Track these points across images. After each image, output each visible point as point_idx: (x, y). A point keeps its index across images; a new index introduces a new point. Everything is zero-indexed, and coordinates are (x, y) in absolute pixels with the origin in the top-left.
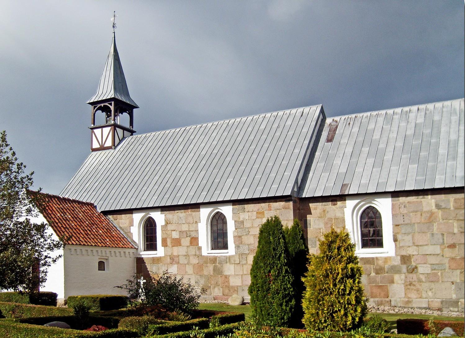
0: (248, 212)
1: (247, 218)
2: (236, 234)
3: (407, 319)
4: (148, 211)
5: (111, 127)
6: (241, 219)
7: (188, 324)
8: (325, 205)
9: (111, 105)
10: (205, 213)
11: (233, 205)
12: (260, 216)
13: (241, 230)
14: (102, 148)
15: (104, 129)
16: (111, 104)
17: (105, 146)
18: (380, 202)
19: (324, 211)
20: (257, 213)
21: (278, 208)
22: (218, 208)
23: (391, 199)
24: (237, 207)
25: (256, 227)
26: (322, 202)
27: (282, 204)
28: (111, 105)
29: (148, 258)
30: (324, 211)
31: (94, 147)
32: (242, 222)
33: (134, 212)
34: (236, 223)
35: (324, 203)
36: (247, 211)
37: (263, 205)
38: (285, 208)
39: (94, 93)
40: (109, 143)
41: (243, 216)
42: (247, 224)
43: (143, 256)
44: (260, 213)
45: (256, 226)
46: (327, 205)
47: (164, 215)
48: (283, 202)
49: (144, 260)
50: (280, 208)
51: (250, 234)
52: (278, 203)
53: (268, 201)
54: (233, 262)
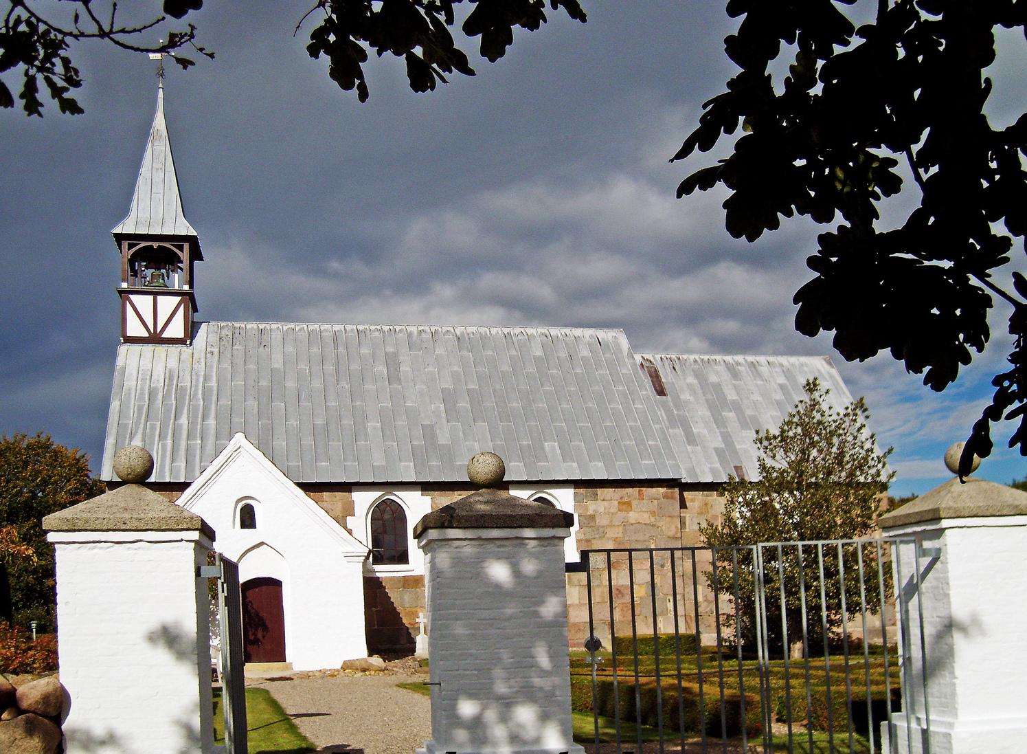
0: (604, 500)
1: (602, 510)
2: (582, 537)
3: (818, 657)
4: (389, 489)
5: (180, 298)
6: (590, 512)
7: (768, 640)
8: (707, 496)
9: (182, 251)
10: (364, 501)
11: (575, 488)
12: (624, 507)
13: (590, 529)
14: (155, 339)
15: (160, 298)
16: (181, 248)
17: (164, 336)
18: (258, 499)
19: (706, 504)
20: (619, 502)
21: (656, 496)
22: (395, 493)
23: (573, 490)
24: (582, 491)
25: (618, 526)
26: (703, 491)
27: (662, 490)
28: (182, 251)
29: (392, 578)
30: (706, 504)
31: (129, 334)
32: (592, 517)
33: (353, 488)
34: (581, 518)
35: (705, 493)
36: (602, 499)
37: (630, 490)
38: (666, 496)
39: (123, 212)
40: (176, 329)
41: (592, 507)
42: (602, 521)
43: (378, 575)
44: (624, 503)
45: (617, 524)
46: (711, 496)
47: (430, 497)
48: (664, 487)
49: (381, 583)
50: (658, 497)
51: (607, 536)
52: (654, 490)
53: (638, 485)
54: (576, 582)
